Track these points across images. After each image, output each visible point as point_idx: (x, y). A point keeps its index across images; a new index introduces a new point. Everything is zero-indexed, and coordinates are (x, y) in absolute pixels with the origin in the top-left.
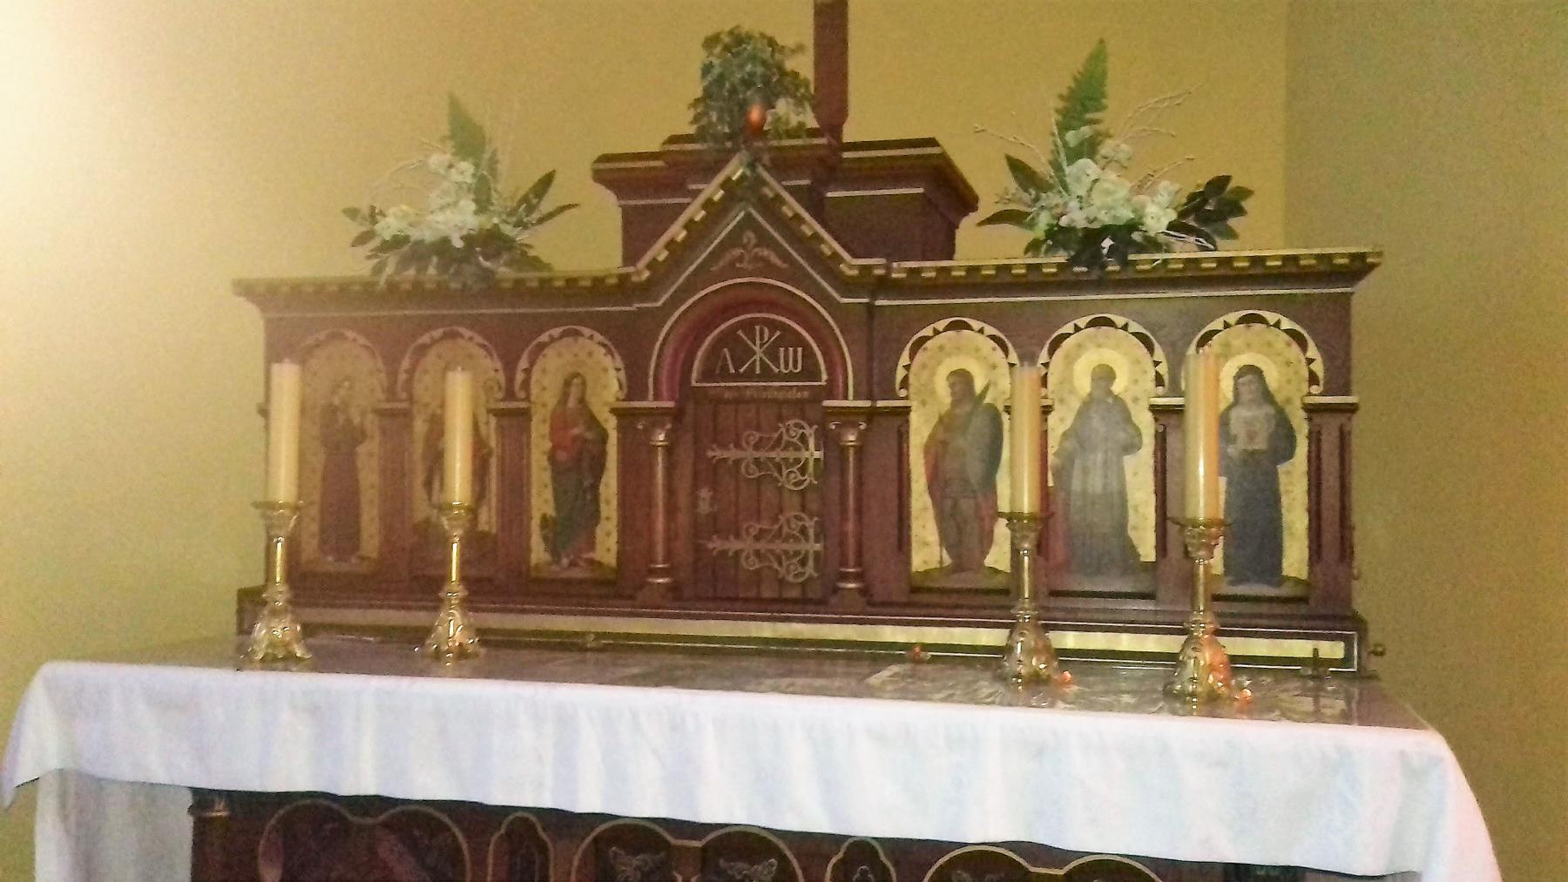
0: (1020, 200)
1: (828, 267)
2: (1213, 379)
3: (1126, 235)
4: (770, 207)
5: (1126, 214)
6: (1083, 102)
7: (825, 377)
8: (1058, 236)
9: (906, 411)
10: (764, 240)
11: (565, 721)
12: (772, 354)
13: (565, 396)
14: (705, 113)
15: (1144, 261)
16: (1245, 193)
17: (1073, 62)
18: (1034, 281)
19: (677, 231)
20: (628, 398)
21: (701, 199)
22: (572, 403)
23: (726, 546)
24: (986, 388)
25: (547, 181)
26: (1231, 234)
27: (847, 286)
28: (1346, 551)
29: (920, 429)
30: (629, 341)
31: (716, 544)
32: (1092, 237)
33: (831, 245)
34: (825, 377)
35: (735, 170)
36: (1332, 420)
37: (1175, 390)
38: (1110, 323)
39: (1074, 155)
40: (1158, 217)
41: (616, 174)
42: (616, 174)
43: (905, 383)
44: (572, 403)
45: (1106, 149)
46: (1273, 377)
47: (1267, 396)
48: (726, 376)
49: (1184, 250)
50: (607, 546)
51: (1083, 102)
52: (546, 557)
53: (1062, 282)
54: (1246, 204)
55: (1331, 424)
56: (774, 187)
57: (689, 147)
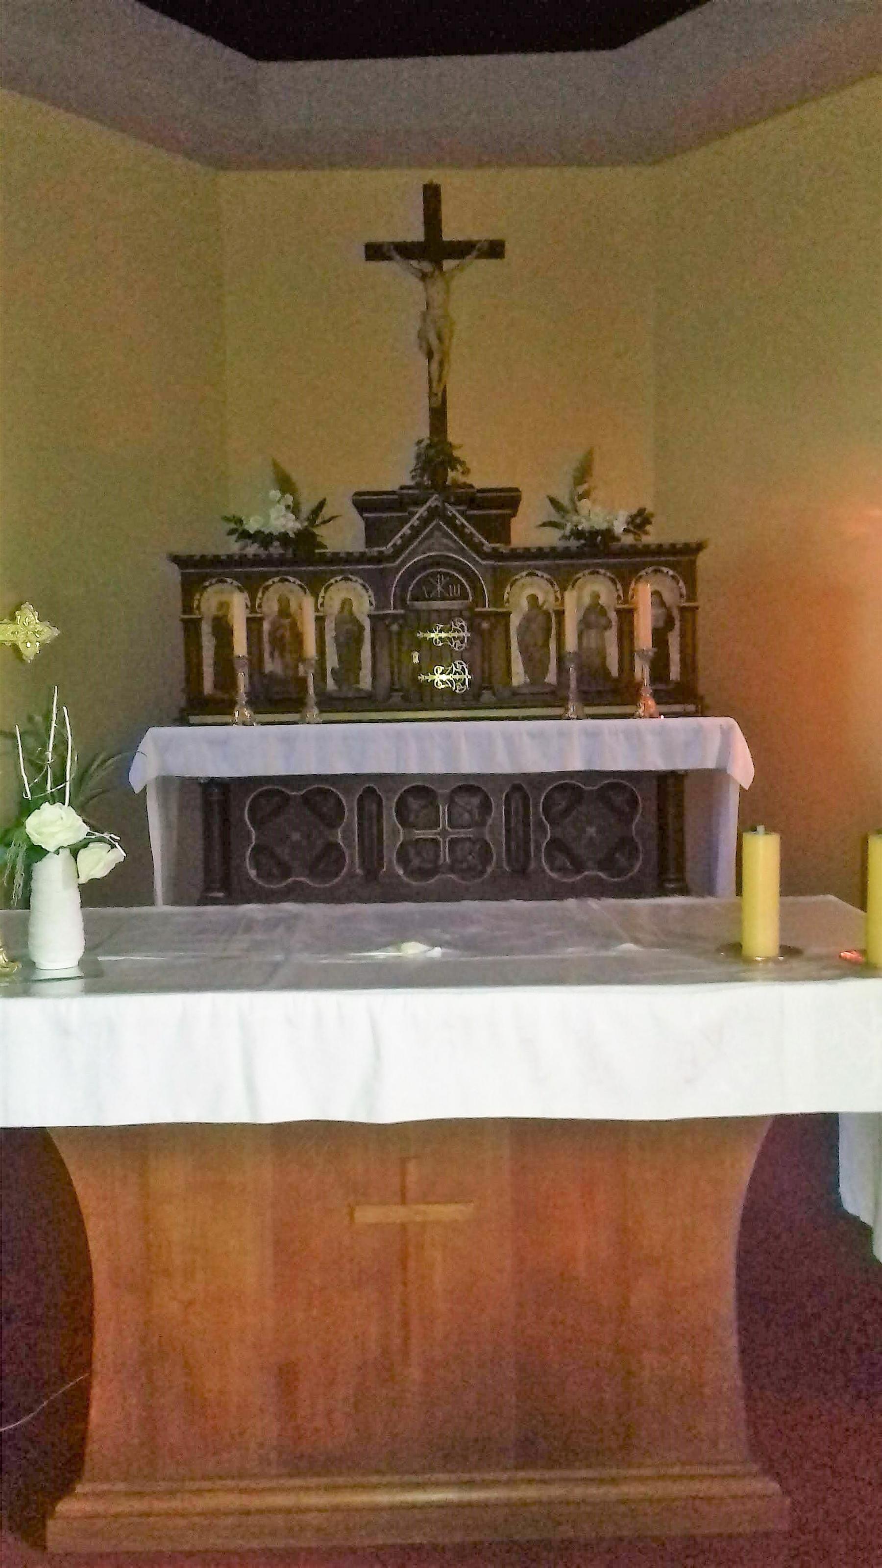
0: (556, 517)
1: (477, 548)
2: (573, 604)
3: (608, 534)
4: (450, 521)
5: (604, 526)
6: (583, 473)
7: (471, 598)
8: (578, 534)
9: (508, 614)
10: (446, 535)
11: (594, 735)
12: (445, 587)
13: (342, 608)
14: (422, 476)
15: (615, 545)
16: (652, 515)
17: (579, 454)
18: (566, 553)
19: (406, 530)
20: (377, 608)
21: (417, 516)
22: (346, 613)
23: (427, 677)
24: (545, 602)
25: (321, 505)
26: (646, 533)
27: (486, 556)
28: (694, 669)
29: (515, 621)
30: (377, 583)
31: (422, 678)
32: (594, 533)
33: (479, 537)
34: (471, 598)
35: (433, 502)
36: (689, 613)
37: (626, 602)
38: (598, 573)
39: (581, 497)
40: (619, 527)
41: (365, 503)
42: (365, 503)
43: (508, 601)
44: (346, 613)
45: (593, 495)
46: (667, 597)
47: (662, 604)
48: (256, 612)
49: (628, 540)
50: (366, 682)
51: (583, 473)
52: (335, 688)
53: (579, 554)
54: (653, 520)
55: (688, 615)
56: (452, 510)
57: (410, 491)
